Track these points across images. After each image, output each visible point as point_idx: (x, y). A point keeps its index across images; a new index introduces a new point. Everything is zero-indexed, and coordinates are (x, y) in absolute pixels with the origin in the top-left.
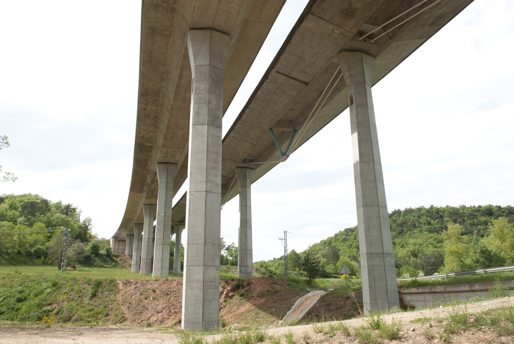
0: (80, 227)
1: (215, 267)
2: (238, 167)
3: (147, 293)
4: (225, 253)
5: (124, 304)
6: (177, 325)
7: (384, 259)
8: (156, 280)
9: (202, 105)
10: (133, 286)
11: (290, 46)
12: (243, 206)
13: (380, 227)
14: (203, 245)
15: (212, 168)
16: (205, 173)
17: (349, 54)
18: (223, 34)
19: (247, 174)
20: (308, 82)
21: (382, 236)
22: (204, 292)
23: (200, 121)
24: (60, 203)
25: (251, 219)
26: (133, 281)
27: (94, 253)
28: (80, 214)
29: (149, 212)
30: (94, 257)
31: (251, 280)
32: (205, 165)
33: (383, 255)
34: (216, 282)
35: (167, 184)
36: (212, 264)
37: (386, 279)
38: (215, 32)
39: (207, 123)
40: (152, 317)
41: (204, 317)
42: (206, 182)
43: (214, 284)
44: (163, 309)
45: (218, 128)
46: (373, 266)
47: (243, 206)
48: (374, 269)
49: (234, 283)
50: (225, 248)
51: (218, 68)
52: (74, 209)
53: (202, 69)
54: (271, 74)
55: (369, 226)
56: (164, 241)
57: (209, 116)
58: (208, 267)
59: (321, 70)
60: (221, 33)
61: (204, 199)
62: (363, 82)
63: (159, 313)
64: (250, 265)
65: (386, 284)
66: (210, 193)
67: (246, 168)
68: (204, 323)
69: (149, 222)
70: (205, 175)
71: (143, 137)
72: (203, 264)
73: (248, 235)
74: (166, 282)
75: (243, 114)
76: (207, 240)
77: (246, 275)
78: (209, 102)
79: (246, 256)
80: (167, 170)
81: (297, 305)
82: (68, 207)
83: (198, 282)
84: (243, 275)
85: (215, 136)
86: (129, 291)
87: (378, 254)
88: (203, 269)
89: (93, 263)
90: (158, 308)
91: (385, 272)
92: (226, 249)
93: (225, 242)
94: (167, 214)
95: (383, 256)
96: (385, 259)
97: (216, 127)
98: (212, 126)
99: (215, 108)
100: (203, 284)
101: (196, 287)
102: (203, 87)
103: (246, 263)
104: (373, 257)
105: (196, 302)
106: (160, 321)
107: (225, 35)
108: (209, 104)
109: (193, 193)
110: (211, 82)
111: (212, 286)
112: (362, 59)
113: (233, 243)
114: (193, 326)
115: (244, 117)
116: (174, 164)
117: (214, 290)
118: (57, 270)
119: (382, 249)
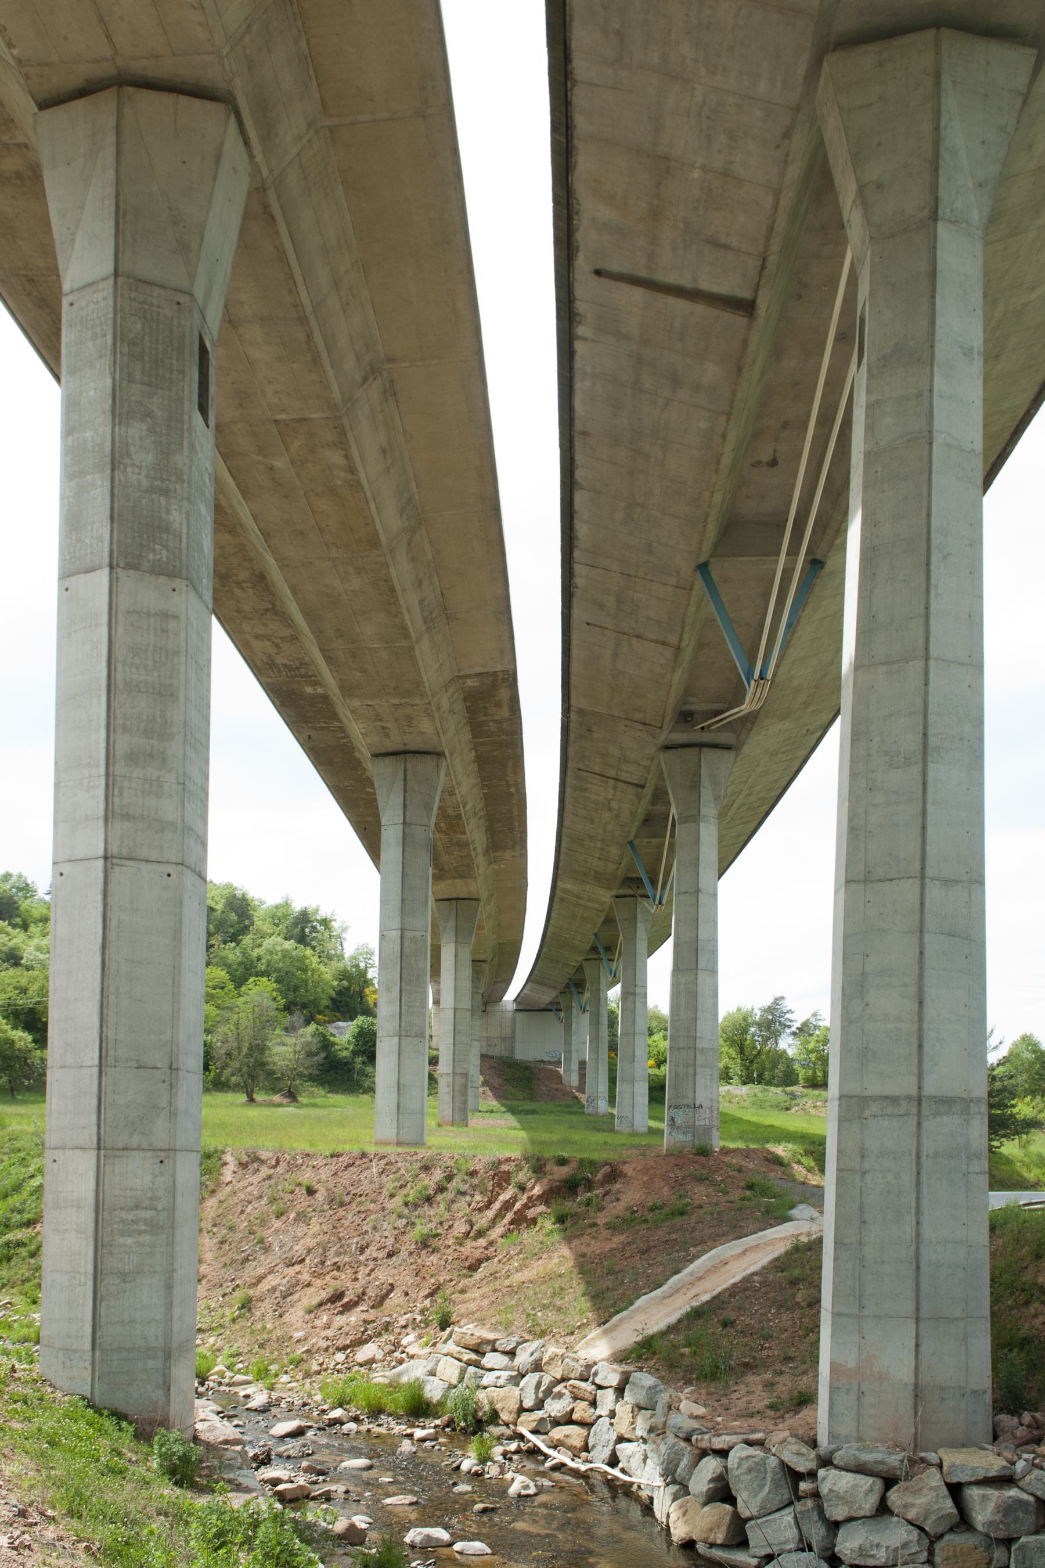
0: (344, 975)
1: (149, 1154)
2: (668, 747)
3: (290, 1197)
4: (789, 1045)
5: (215, 1230)
6: (324, 1308)
7: (919, 1124)
8: (332, 1156)
9: (89, 477)
10: (265, 1171)
11: (579, 97)
12: (686, 892)
13: (921, 976)
14: (95, 1071)
15: (133, 758)
16: (102, 781)
17: (866, 57)
18: (183, 100)
19: (704, 771)
20: (746, 294)
21: (921, 1020)
22: (100, 1244)
23: (83, 552)
24: (287, 904)
25: (714, 940)
26: (271, 1155)
27: (364, 1052)
28: (344, 935)
29: (454, 923)
30: (364, 1063)
31: (625, 1163)
32: (103, 745)
33: (919, 1104)
34: (156, 1209)
35: (407, 830)
36: (135, 1140)
37: (918, 1212)
38: (144, 92)
39: (107, 559)
40: (270, 1277)
41: (99, 1334)
42: (106, 819)
43: (148, 1214)
44: (309, 1251)
45: (162, 579)
46: (862, 1156)
47: (686, 892)
48: (867, 1165)
49: (564, 1171)
50: (788, 1031)
51: (162, 286)
52: (325, 922)
53: (87, 305)
54: (579, 291)
55: (864, 974)
56: (403, 1024)
57: (115, 525)
58: (117, 1153)
59: (776, 207)
60: (173, 96)
61: (100, 887)
62: (926, 212)
63: (293, 1265)
64: (706, 1104)
65: (918, 1234)
66: (127, 863)
67: (701, 745)
68: (98, 1353)
69: (456, 956)
70: (101, 792)
71: (271, 664)
72: (95, 1141)
73: (700, 999)
74: (357, 1163)
75: (572, 518)
76: (111, 1052)
77: (689, 1138)
78: (116, 461)
79: (691, 1070)
80: (405, 779)
81: (691, 1274)
82: (304, 918)
83: (78, 1207)
84: (680, 1137)
85: (148, 614)
86: (246, 1187)
87: (893, 1100)
88: (94, 1161)
89: (358, 1081)
90: (296, 1248)
91: (918, 1184)
92: (794, 1034)
93: (790, 1011)
94: (409, 935)
95: (914, 1111)
96: (925, 1124)
97: (152, 572)
98: (132, 572)
99: (145, 483)
100: (93, 1215)
101: (74, 1226)
102: (92, 393)
103: (691, 1095)
104: (867, 1113)
105: (75, 1278)
106: (281, 1292)
107: (198, 103)
108: (113, 470)
109: (66, 868)
110: (126, 359)
111: (135, 1222)
112: (937, 76)
113: (815, 1015)
114: (64, 1363)
115: (582, 530)
116: (428, 757)
117: (146, 1238)
118: (243, 1105)
119: (914, 1080)
